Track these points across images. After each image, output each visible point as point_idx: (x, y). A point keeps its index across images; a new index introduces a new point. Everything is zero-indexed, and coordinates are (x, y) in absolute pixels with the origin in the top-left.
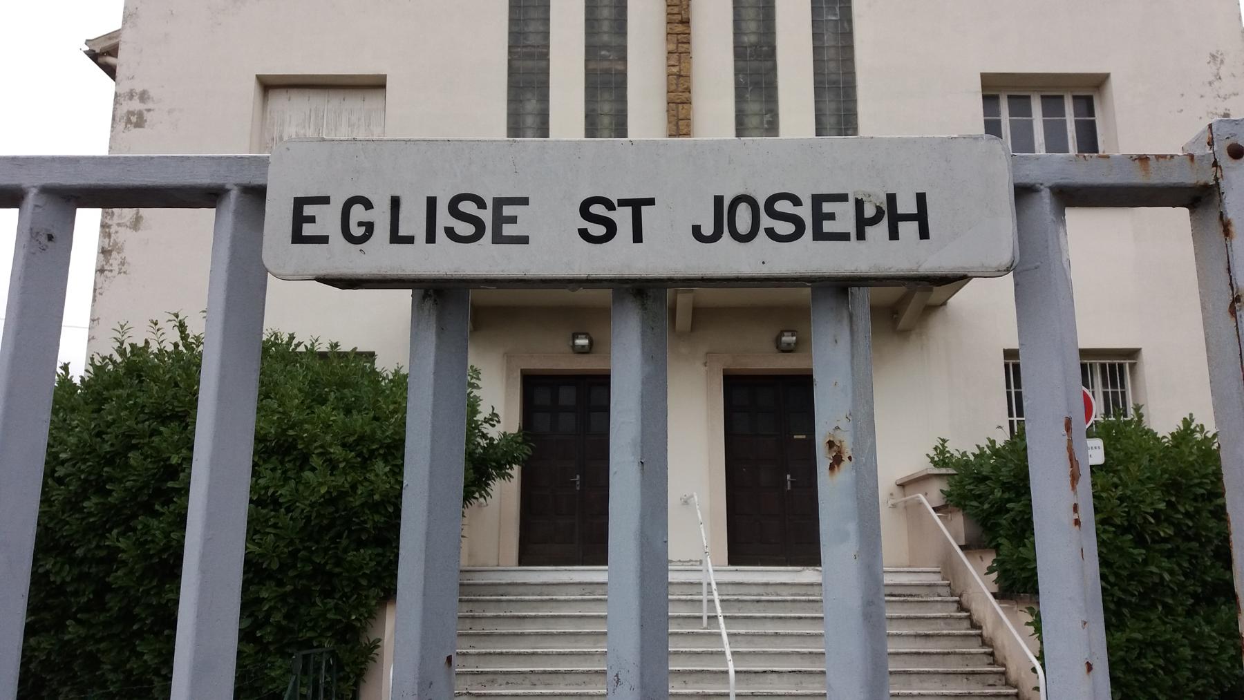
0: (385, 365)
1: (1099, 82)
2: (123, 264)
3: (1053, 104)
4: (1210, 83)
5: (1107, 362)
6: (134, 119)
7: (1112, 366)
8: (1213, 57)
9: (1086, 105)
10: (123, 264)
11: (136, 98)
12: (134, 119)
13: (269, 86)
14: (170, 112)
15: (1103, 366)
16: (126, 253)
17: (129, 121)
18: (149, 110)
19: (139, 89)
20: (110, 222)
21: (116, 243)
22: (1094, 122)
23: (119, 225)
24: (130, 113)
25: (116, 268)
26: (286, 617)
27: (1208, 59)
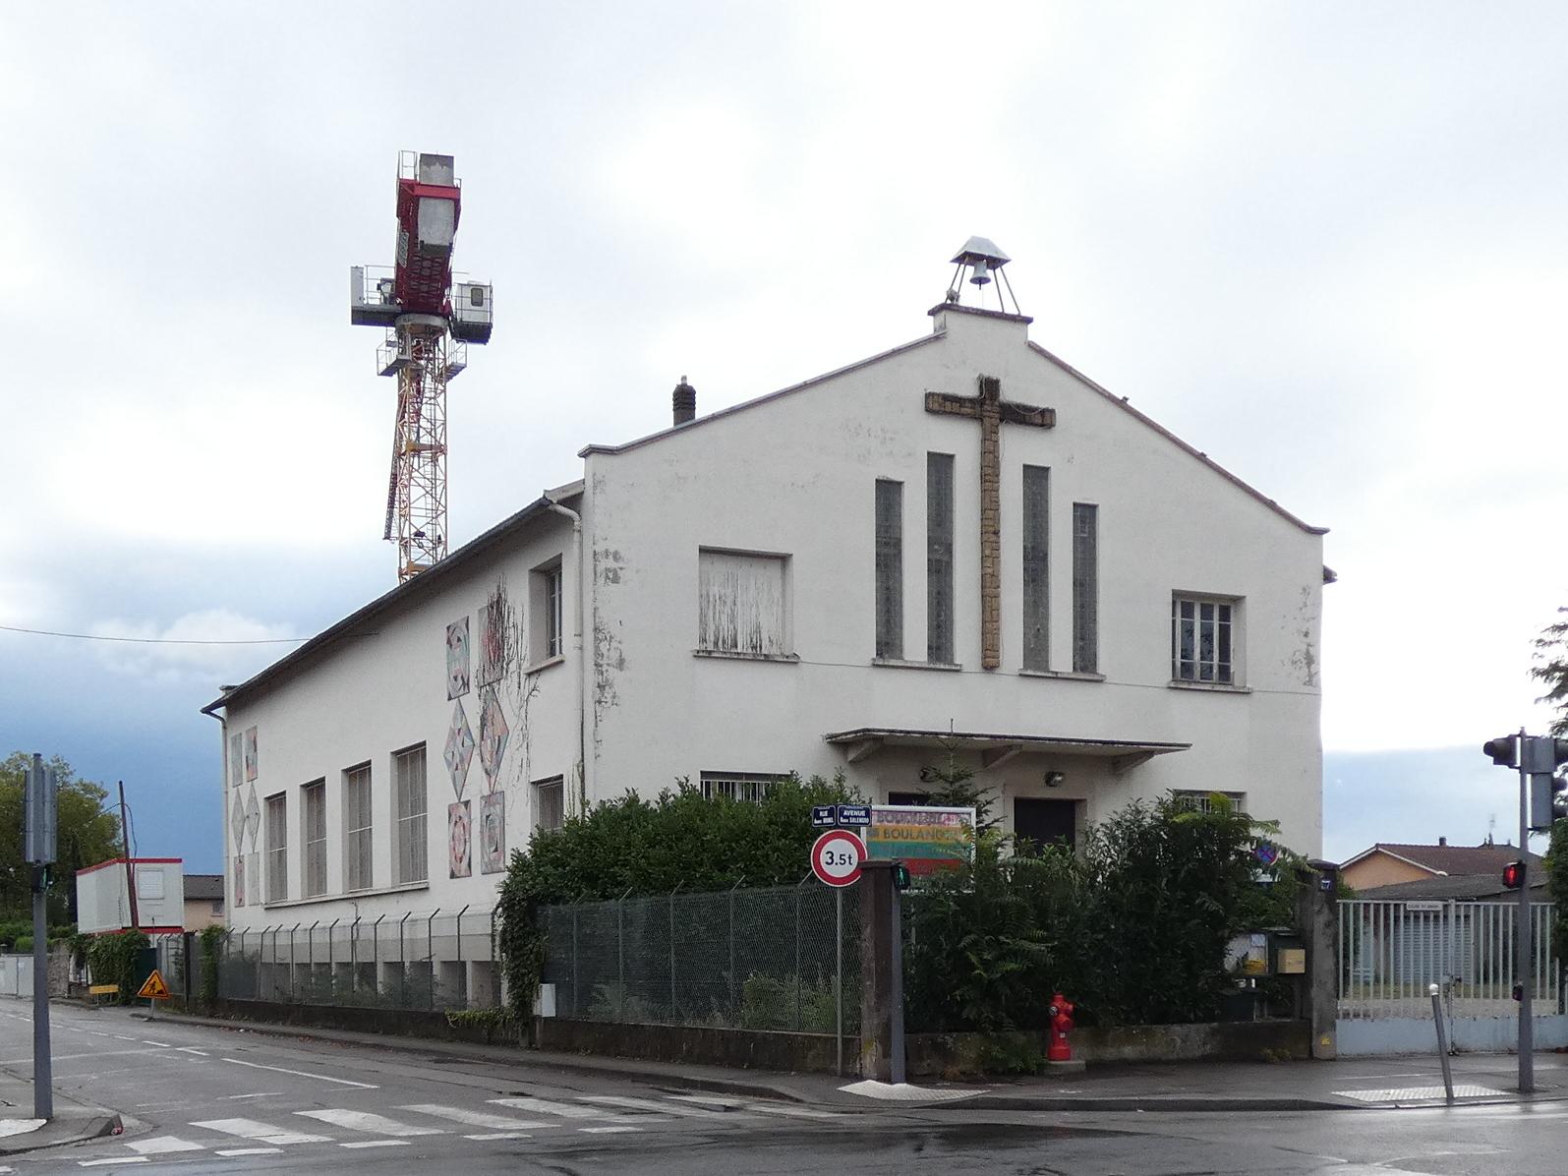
0: (830, 781)
1: (1238, 600)
2: (614, 697)
3: (1207, 613)
4: (1301, 609)
5: (731, 781)
6: (611, 575)
7: (727, 784)
8: (1304, 589)
9: (1225, 614)
10: (614, 697)
11: (611, 557)
12: (611, 575)
13: (705, 551)
14: (637, 571)
15: (721, 784)
16: (616, 688)
17: (607, 577)
18: (621, 569)
19: (612, 550)
20: (601, 662)
21: (607, 680)
22: (1229, 626)
23: (608, 665)
24: (607, 570)
25: (609, 700)
26: (727, 969)
27: (1301, 591)
